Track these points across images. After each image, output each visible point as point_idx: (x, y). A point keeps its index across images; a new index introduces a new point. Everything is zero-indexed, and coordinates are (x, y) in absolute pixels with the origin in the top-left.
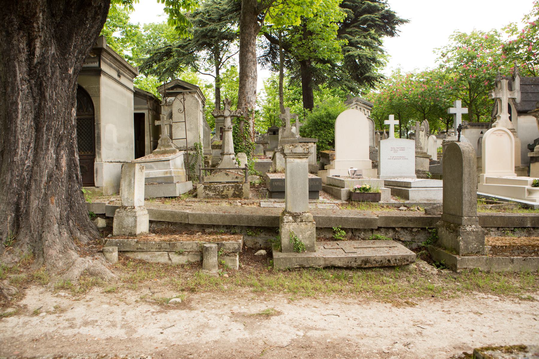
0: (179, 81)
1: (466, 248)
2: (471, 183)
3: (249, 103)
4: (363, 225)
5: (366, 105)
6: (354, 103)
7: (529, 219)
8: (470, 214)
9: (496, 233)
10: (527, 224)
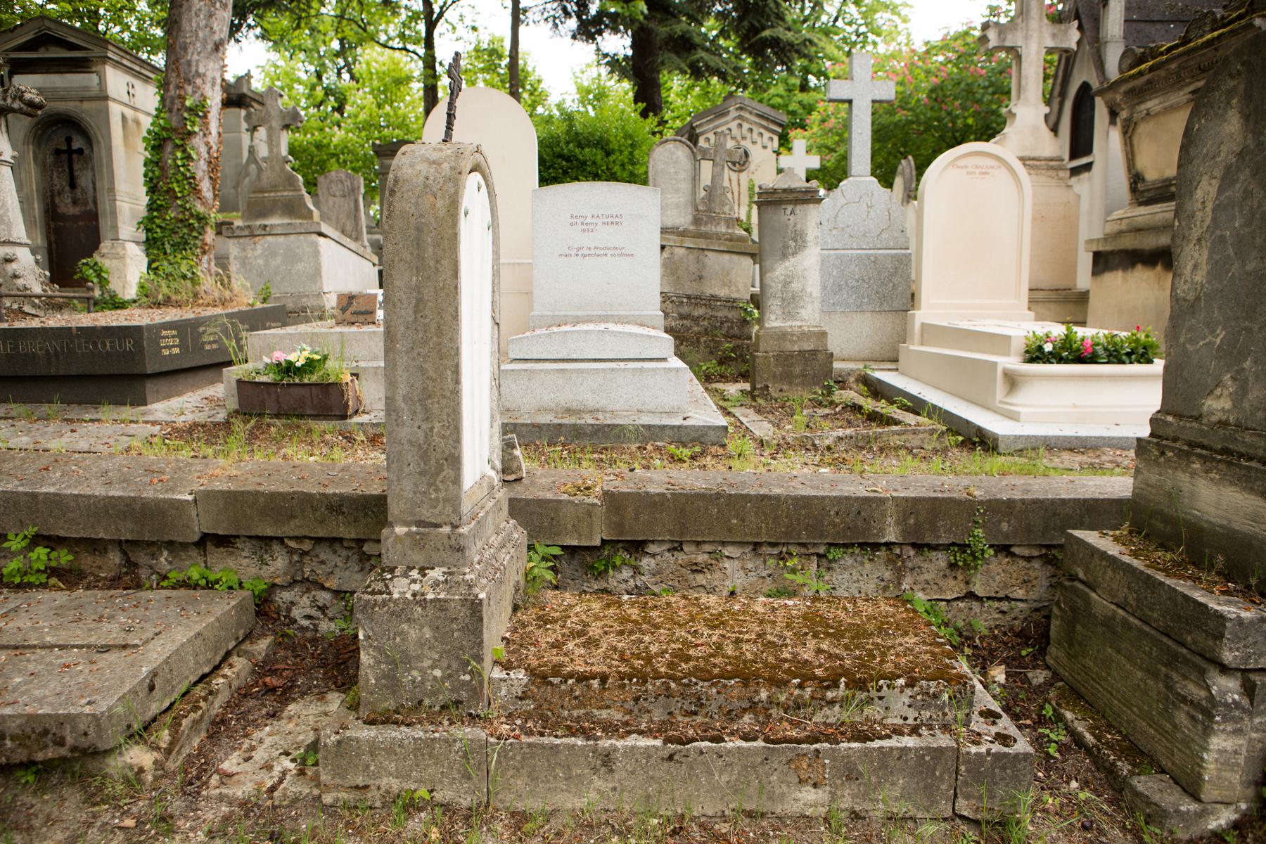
0: (48, 24)
1: (391, 682)
2: (424, 351)
3: (189, 81)
4: (130, 525)
5: (767, 119)
6: (733, 113)
7: (890, 508)
8: (426, 514)
9: (750, 565)
10: (882, 530)
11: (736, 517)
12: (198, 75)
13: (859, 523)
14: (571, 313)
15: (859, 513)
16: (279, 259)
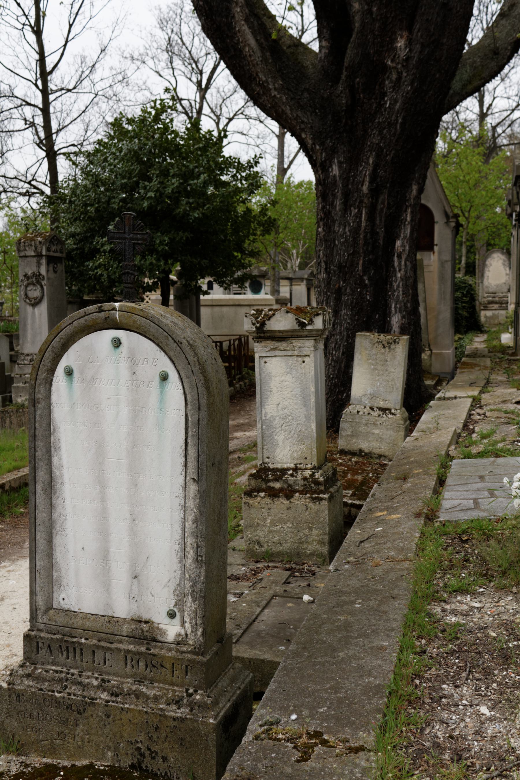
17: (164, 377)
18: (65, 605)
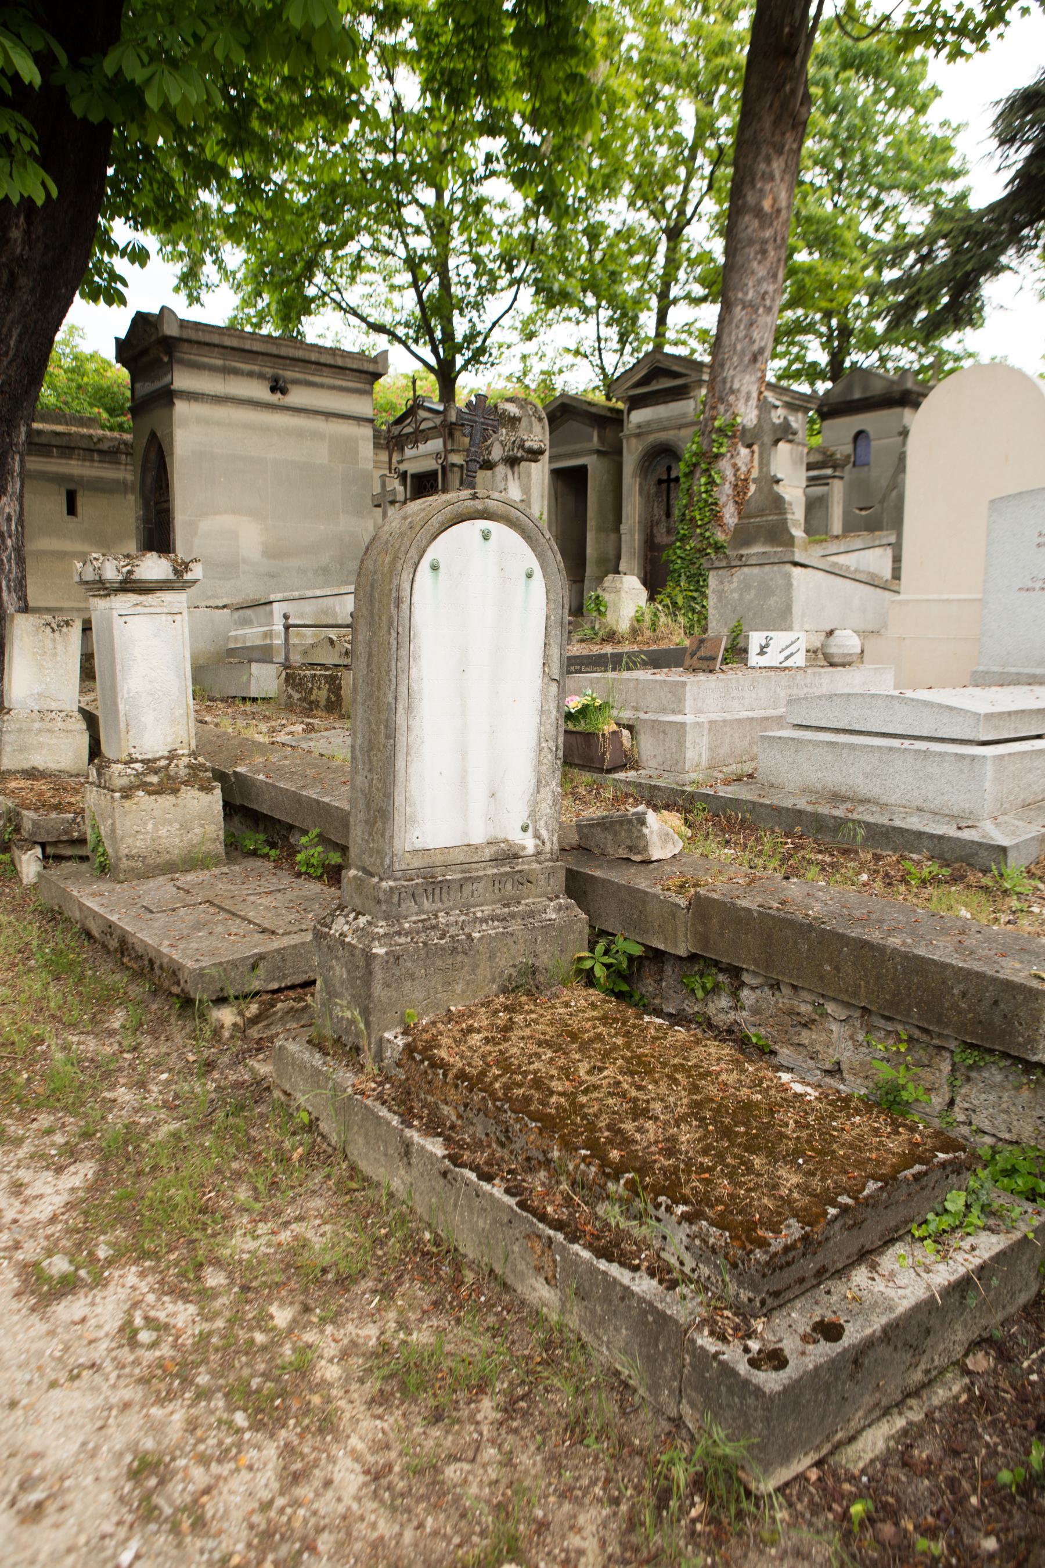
11: (830, 962)
12: (732, 391)
13: (997, 1020)
14: (1027, 670)
15: (996, 1003)
16: (753, 592)
17: (529, 576)
18: (419, 845)
